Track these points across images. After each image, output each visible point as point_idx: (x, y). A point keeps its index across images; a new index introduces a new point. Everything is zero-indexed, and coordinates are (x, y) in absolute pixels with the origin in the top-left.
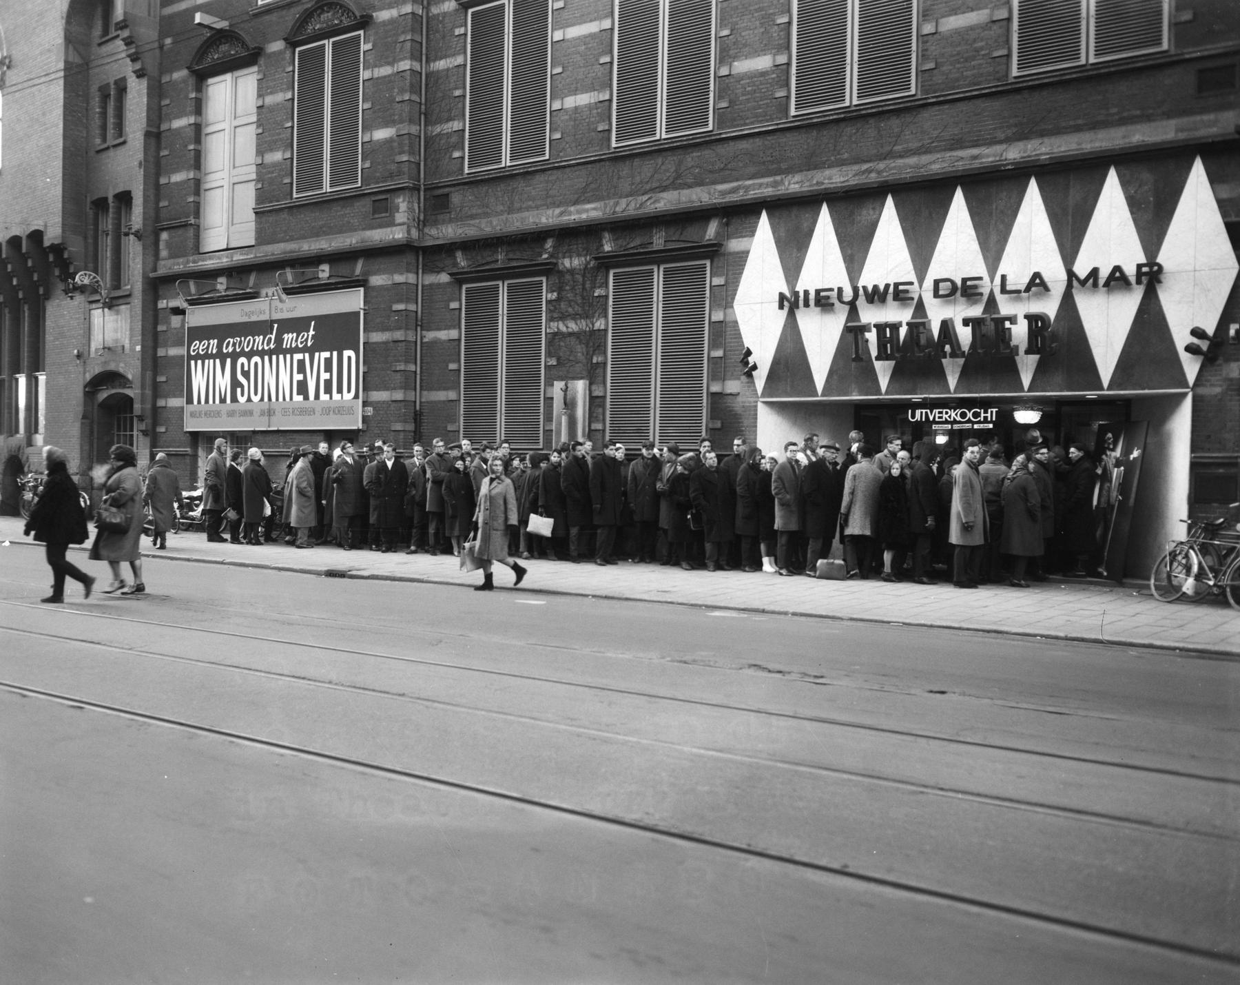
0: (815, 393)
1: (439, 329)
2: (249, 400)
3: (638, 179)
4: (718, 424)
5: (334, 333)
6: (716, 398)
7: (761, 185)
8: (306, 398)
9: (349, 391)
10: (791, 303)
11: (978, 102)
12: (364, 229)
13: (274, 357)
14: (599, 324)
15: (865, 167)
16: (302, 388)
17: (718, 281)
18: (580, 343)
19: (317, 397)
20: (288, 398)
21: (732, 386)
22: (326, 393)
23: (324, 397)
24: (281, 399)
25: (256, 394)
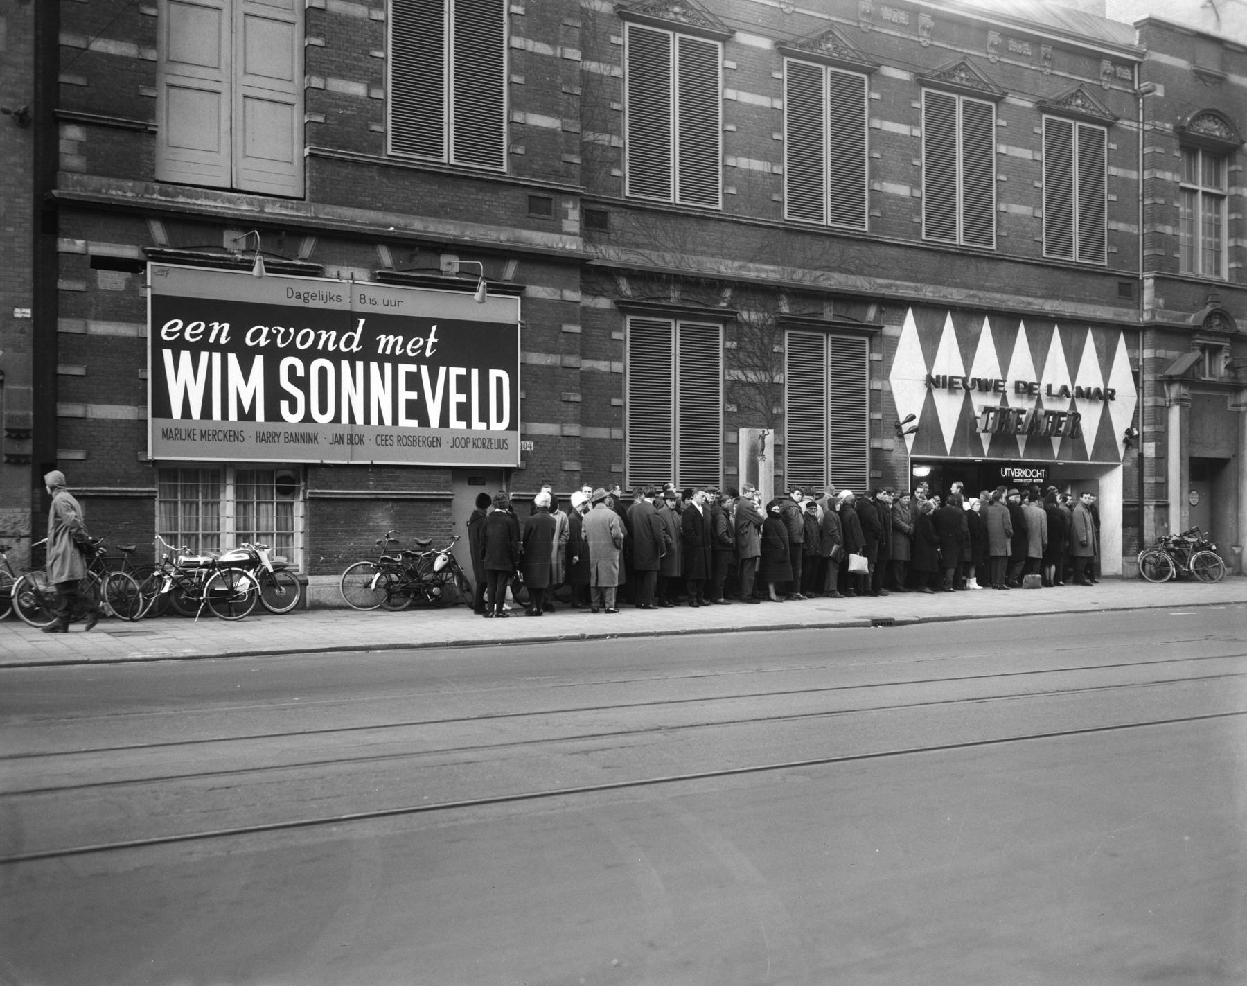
0: (945, 453)
1: (598, 359)
2: (308, 418)
3: (809, 255)
4: (879, 474)
5: (471, 345)
6: (876, 451)
7: (907, 287)
8: (424, 422)
9: (500, 419)
10: (933, 383)
11: (1029, 267)
12: (515, 226)
13: (360, 365)
14: (777, 379)
15: (972, 292)
16: (417, 410)
17: (876, 357)
18: (760, 393)
19: (444, 421)
20: (388, 421)
21: (889, 443)
22: (459, 419)
23: (455, 424)
24: (374, 420)
25: (323, 410)
